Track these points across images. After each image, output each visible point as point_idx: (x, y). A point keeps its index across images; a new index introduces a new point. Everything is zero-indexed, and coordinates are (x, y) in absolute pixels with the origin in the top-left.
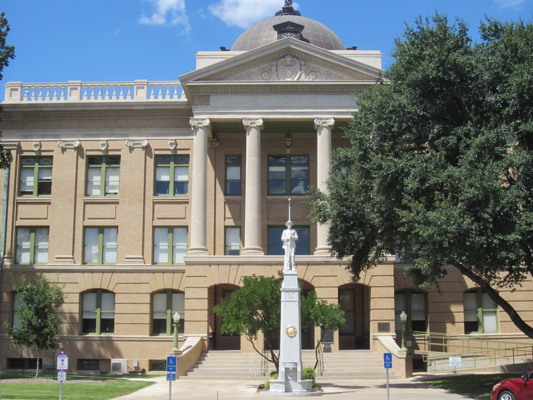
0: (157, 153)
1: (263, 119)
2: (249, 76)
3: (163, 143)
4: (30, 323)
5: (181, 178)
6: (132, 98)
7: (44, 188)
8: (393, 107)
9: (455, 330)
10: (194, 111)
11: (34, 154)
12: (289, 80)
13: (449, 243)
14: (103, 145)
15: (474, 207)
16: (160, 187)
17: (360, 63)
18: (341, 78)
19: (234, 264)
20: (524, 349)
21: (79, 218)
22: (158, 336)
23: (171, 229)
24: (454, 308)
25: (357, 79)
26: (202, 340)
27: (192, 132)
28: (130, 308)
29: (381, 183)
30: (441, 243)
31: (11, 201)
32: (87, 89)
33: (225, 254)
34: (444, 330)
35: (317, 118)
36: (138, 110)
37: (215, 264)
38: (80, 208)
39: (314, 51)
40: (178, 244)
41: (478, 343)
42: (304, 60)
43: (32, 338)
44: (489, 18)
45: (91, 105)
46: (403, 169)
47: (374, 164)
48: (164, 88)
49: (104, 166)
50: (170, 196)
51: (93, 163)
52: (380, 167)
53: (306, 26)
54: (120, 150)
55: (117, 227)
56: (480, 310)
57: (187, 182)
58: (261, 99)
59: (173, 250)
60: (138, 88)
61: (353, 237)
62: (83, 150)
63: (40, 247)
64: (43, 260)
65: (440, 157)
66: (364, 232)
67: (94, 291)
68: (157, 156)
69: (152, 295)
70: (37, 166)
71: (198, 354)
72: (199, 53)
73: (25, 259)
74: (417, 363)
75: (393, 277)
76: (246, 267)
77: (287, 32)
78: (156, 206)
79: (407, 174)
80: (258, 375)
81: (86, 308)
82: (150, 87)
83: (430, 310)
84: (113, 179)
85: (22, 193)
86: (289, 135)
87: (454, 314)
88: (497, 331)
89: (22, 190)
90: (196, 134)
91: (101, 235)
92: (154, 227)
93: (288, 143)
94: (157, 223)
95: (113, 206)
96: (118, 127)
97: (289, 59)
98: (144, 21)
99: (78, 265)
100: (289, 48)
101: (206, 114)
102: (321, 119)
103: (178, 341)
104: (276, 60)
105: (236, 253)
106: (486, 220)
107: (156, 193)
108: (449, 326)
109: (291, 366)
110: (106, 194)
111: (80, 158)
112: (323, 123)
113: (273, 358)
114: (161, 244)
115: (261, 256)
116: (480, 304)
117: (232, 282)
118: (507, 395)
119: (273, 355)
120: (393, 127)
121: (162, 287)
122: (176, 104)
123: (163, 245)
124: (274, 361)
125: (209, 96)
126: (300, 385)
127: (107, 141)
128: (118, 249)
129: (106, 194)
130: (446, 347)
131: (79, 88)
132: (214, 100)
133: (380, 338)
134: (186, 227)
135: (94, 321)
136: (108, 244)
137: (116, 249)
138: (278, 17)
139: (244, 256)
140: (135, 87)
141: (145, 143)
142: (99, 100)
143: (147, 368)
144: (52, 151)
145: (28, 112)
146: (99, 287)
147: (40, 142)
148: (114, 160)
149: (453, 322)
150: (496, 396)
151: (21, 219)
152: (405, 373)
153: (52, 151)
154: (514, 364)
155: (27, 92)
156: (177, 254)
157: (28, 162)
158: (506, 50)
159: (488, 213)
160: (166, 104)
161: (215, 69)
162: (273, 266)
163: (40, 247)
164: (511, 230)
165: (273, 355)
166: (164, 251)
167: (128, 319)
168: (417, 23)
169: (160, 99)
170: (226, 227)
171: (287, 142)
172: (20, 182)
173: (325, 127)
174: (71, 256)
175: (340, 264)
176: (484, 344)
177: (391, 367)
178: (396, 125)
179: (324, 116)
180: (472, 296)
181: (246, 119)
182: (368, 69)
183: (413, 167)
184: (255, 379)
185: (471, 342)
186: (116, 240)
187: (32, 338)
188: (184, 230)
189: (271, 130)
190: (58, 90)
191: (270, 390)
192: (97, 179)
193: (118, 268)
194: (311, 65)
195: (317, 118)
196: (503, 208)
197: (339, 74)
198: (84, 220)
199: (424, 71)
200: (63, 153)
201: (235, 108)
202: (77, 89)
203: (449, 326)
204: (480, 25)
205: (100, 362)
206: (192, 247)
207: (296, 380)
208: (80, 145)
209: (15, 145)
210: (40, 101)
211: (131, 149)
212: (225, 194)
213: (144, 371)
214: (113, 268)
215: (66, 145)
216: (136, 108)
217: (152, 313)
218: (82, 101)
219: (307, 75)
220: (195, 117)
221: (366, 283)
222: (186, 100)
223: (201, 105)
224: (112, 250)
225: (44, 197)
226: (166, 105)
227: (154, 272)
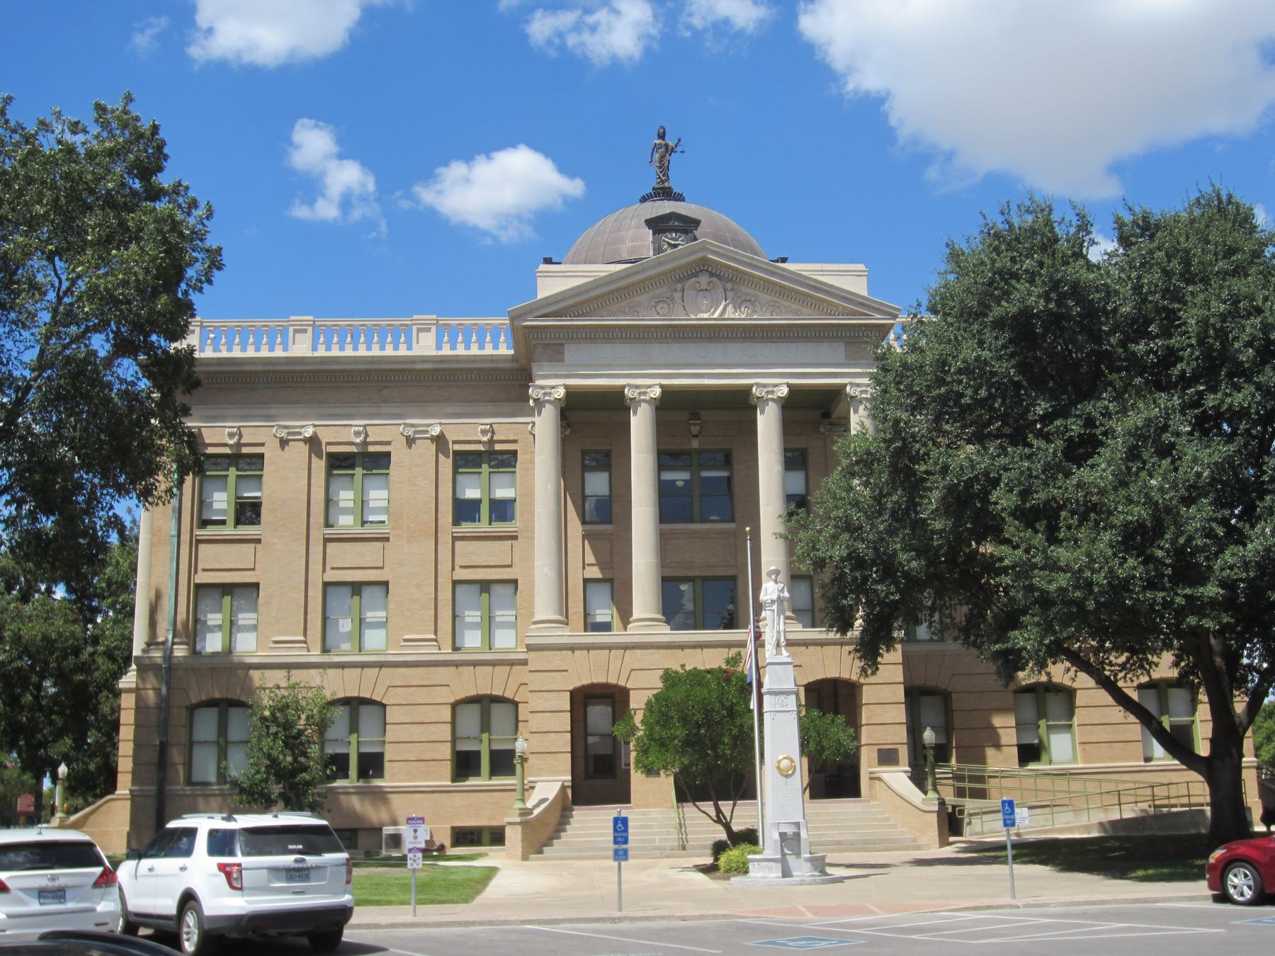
0: (458, 447)
1: (661, 386)
2: (634, 310)
3: (469, 430)
4: (274, 762)
5: (502, 493)
6: (410, 348)
7: (248, 512)
8: (964, 361)
9: (1002, 760)
10: (536, 371)
11: (227, 451)
12: (706, 316)
13: (1097, 602)
14: (357, 434)
15: (1136, 539)
16: (465, 511)
17: (831, 286)
18: (797, 312)
20: (1133, 792)
21: (316, 567)
22: (467, 783)
23: (485, 586)
24: (998, 721)
25: (826, 314)
26: (563, 788)
27: (532, 409)
28: (417, 733)
29: (944, 498)
30: (1080, 604)
31: (185, 537)
32: (324, 332)
33: (586, 630)
34: (982, 760)
35: (758, 385)
36: (421, 371)
38: (316, 550)
39: (750, 265)
40: (498, 613)
41: (1045, 783)
42: (731, 280)
43: (276, 789)
44: (1130, 204)
45: (457, 359)
46: (986, 473)
47: (936, 463)
48: (481, 332)
49: (359, 471)
50: (483, 526)
51: (340, 467)
52: (945, 470)
53: (703, 220)
54: (388, 443)
55: (385, 584)
56: (1042, 723)
57: (514, 500)
58: (656, 350)
59: (489, 625)
60: (419, 330)
61: (878, 595)
62: (320, 444)
63: (241, 622)
64: (247, 646)
65: (1055, 451)
66: (896, 583)
67: (346, 701)
68: (457, 454)
69: (455, 706)
70: (233, 472)
71: (558, 814)
73: (213, 643)
74: (951, 823)
75: (901, 667)
76: (638, 652)
77: (670, 231)
78: (458, 544)
79: (995, 483)
80: (672, 849)
81: (461, 732)
82: (442, 329)
83: (957, 723)
84: (377, 496)
85: (204, 523)
86: (695, 415)
87: (1000, 731)
88: (1074, 759)
89: (205, 517)
90: (539, 414)
92: (455, 583)
93: (695, 429)
94: (461, 574)
95: (379, 545)
96: (385, 401)
97: (704, 279)
98: (301, 212)
99: (315, 656)
100: (704, 259)
101: (557, 376)
102: (764, 386)
103: (524, 790)
104: (680, 280)
105: (606, 627)
106: (1159, 561)
107: (457, 521)
108: (990, 752)
109: (790, 830)
110: (363, 523)
111: (314, 459)
112: (768, 393)
113: (717, 816)
114: (467, 613)
115: (664, 633)
116: (1042, 714)
117: (612, 681)
118: (1242, 870)
119: (718, 811)
120: (962, 395)
121: (473, 693)
122: (491, 359)
123: (472, 616)
124: (718, 821)
125: (562, 345)
126: (809, 864)
127: (365, 426)
128: (390, 624)
129: (363, 523)
131: (310, 329)
132: (570, 352)
133: (884, 776)
134: (515, 582)
135: (477, 754)
136: (369, 614)
137: (383, 625)
138: (648, 204)
139: (635, 632)
140: (415, 328)
141: (436, 431)
142: (349, 352)
143: (447, 843)
144: (262, 445)
145: (218, 373)
146: (356, 694)
147: (239, 428)
148: (377, 462)
149: (998, 746)
150: (1218, 873)
151: (204, 570)
152: (937, 838)
153: (262, 445)
154: (1122, 820)
155: (212, 336)
157: (216, 466)
158: (1169, 261)
159: (1162, 548)
160: (474, 359)
161: (575, 296)
162: (811, 648)
163: (241, 622)
164: (1203, 581)
165: (718, 811)
166: (474, 626)
167: (412, 752)
168: (1002, 213)
169: (461, 351)
170: (586, 581)
171: (693, 428)
172: (201, 502)
173: (772, 400)
174: (302, 638)
175: (842, 644)
176: (1061, 784)
177: (1013, 825)
178: (969, 392)
179: (771, 381)
180: (1028, 698)
181: (630, 386)
182: (847, 296)
183: (1006, 469)
184: (668, 857)
185: (1038, 781)
186: (513, 605)
187: (276, 789)
188: (510, 589)
189: (676, 408)
190: (396, 332)
191: (751, 874)
192: (346, 497)
193: (392, 659)
194: (744, 289)
195: (757, 384)
196: (1190, 539)
197: (794, 306)
198: (324, 571)
199: (1022, 300)
200: (283, 448)
201: (610, 366)
202: (305, 331)
203: (990, 752)
204: (1113, 218)
205: (359, 834)
207: (798, 854)
208: (315, 433)
210: (237, 353)
211: (410, 441)
212: (584, 522)
213: (442, 848)
214: (382, 658)
215: (289, 434)
216: (418, 366)
217: (454, 740)
218: (316, 354)
220: (539, 382)
221: (622, 683)
222: (512, 352)
223: (549, 361)
225: (247, 531)
226: (474, 361)
227: (457, 664)
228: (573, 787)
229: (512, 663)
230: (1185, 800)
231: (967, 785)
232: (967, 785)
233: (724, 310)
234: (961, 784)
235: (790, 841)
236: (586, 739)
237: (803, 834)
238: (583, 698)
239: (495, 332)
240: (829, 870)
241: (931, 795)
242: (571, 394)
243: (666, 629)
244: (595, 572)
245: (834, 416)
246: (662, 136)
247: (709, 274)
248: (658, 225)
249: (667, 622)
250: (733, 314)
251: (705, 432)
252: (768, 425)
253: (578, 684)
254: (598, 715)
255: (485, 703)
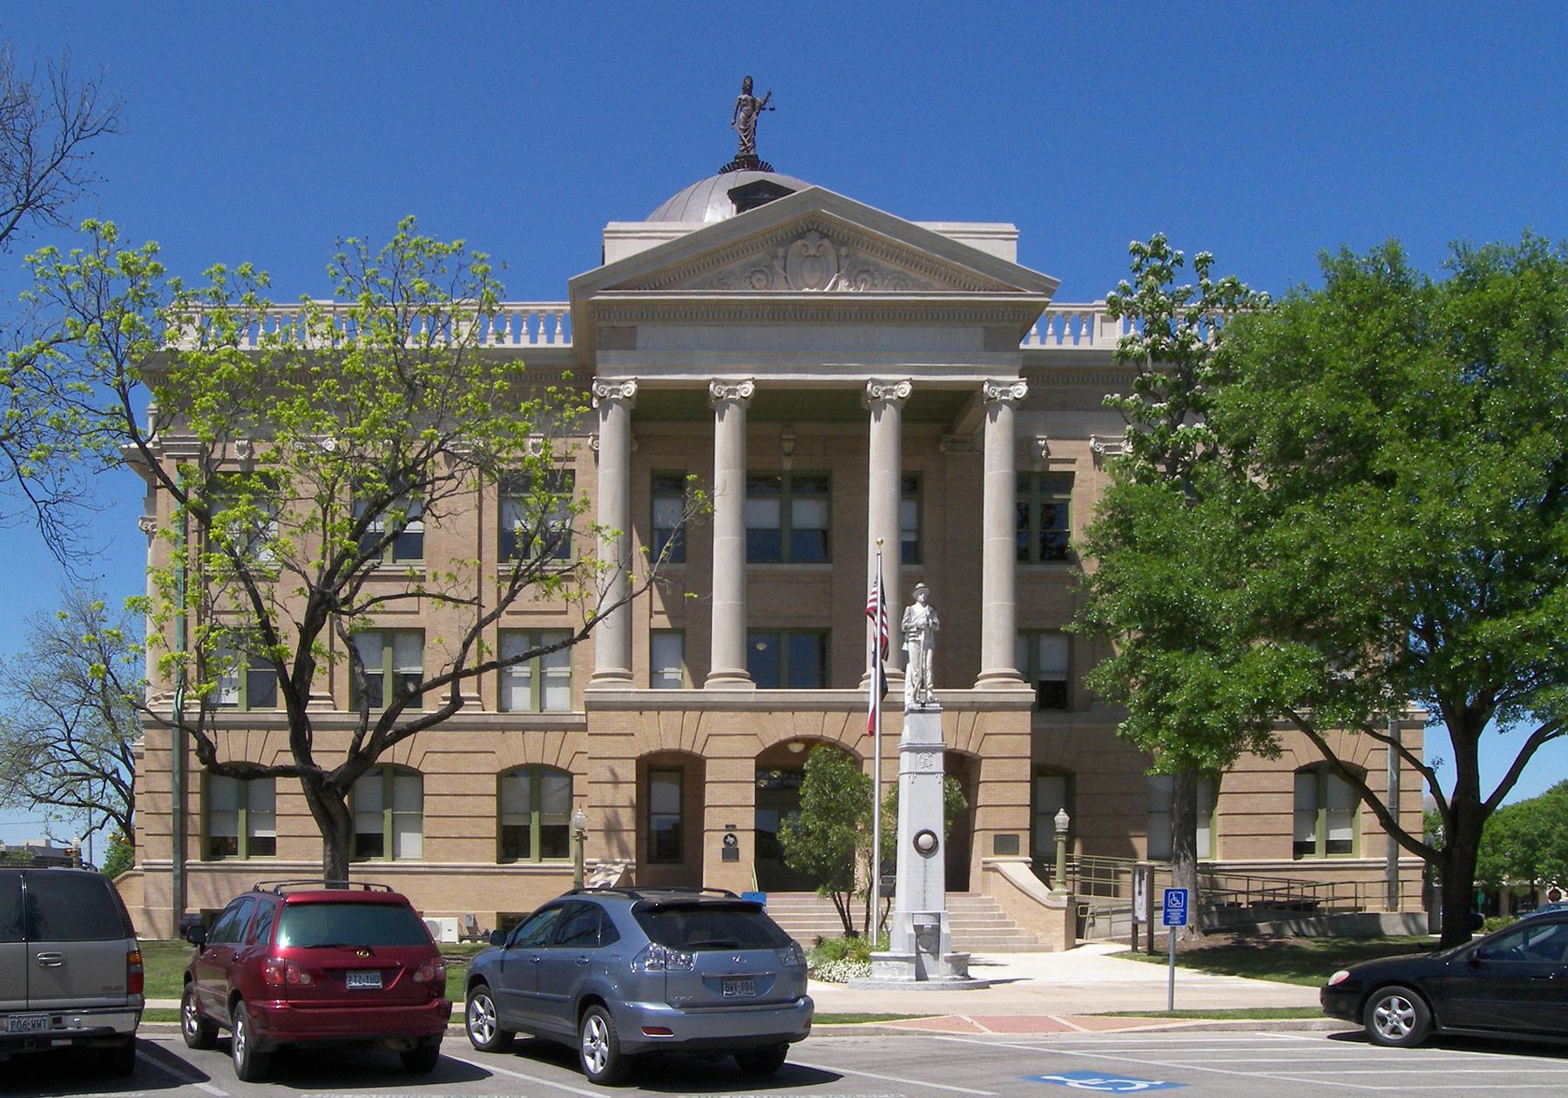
2: (723, 282)
19: (691, 709)
37: (650, 709)
72: (612, 226)
76: (717, 715)
91: (388, 651)
93: (788, 446)
97: (811, 245)
109: (928, 923)
115: (749, 690)
117: (686, 747)
130: (1116, 888)
133: (1002, 866)
137: (567, 681)
156: (514, 689)
173: (890, 401)
188: (415, 638)
197: (923, 279)
206: (598, 671)
207: (936, 953)
209: (194, 448)
219: (853, 281)
221: (697, 750)
224: (558, 682)
228: (638, 871)
229: (565, 728)
230: (1351, 903)
231: (1093, 880)
232: (1093, 880)
233: (836, 284)
234: (1087, 879)
235: (928, 938)
236: (649, 818)
237: (945, 929)
238: (652, 768)
239: (551, 320)
240: (972, 971)
241: (1058, 889)
242: (645, 393)
243: (752, 687)
244: (663, 622)
245: (958, 431)
246: (748, 90)
247: (818, 235)
248: (742, 197)
249: (752, 679)
250: (842, 288)
251: (805, 445)
252: (882, 435)
253: (646, 751)
254: (666, 795)
255: (537, 773)
